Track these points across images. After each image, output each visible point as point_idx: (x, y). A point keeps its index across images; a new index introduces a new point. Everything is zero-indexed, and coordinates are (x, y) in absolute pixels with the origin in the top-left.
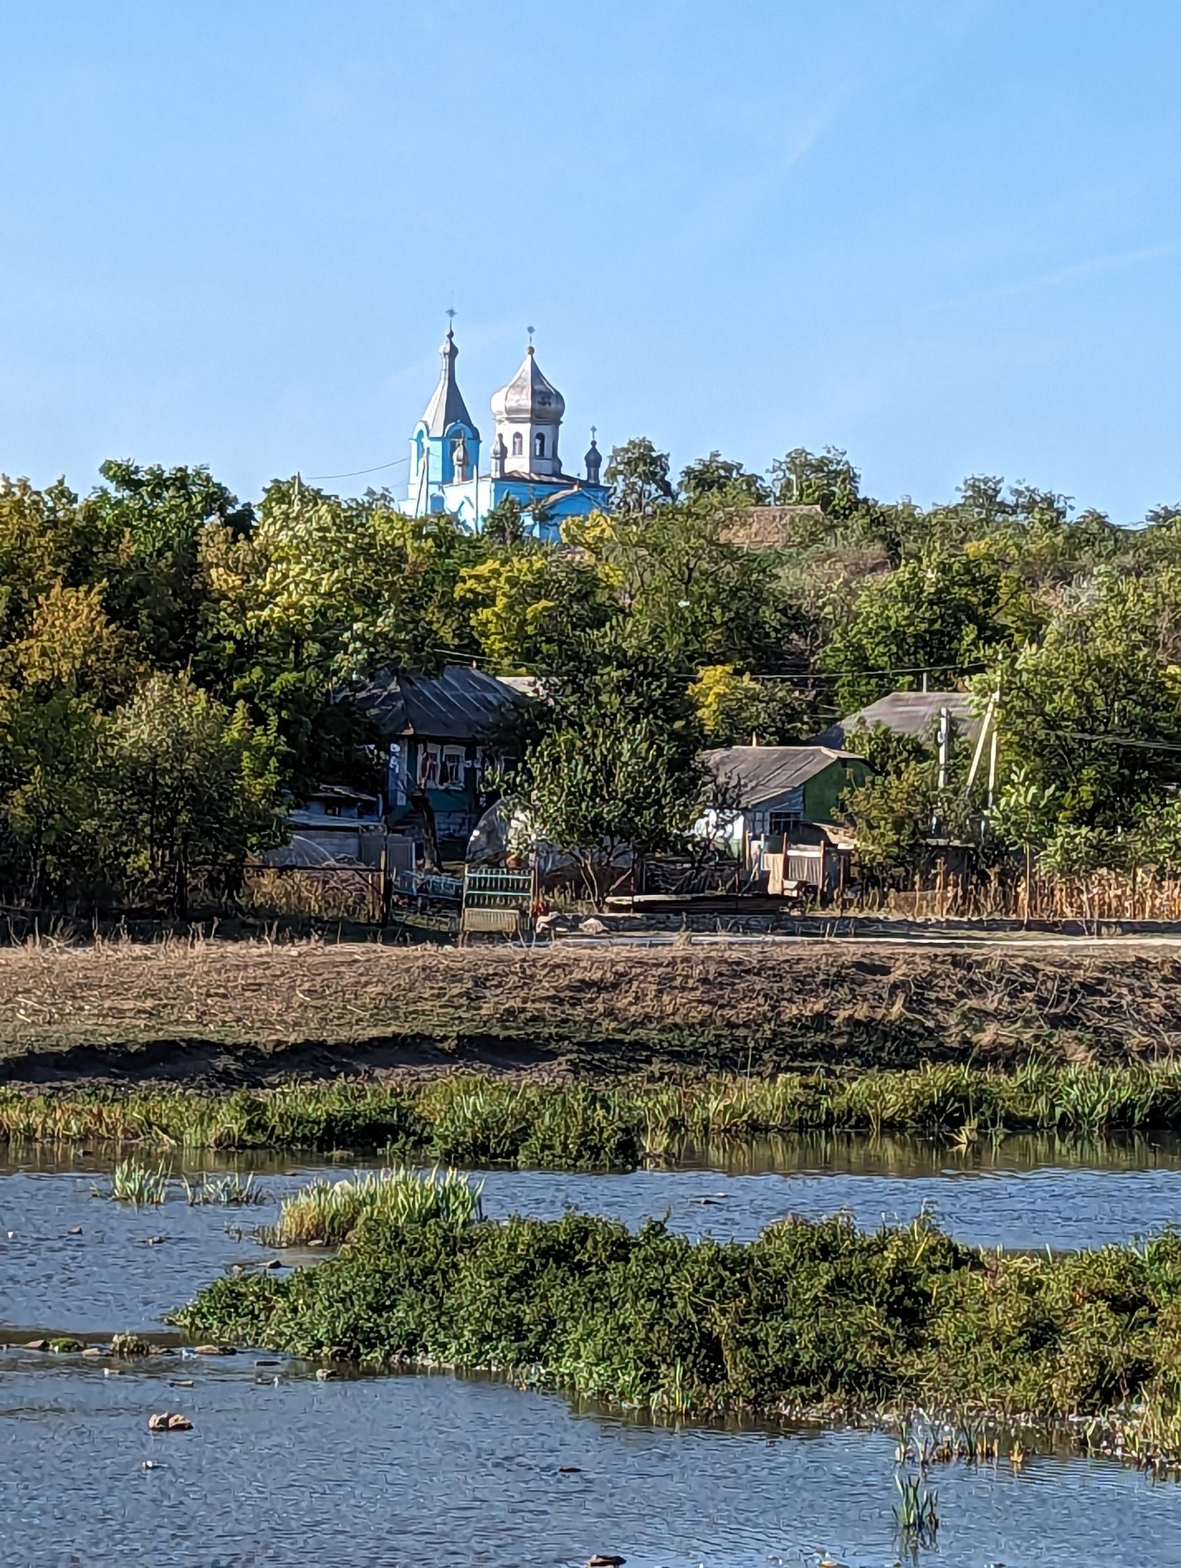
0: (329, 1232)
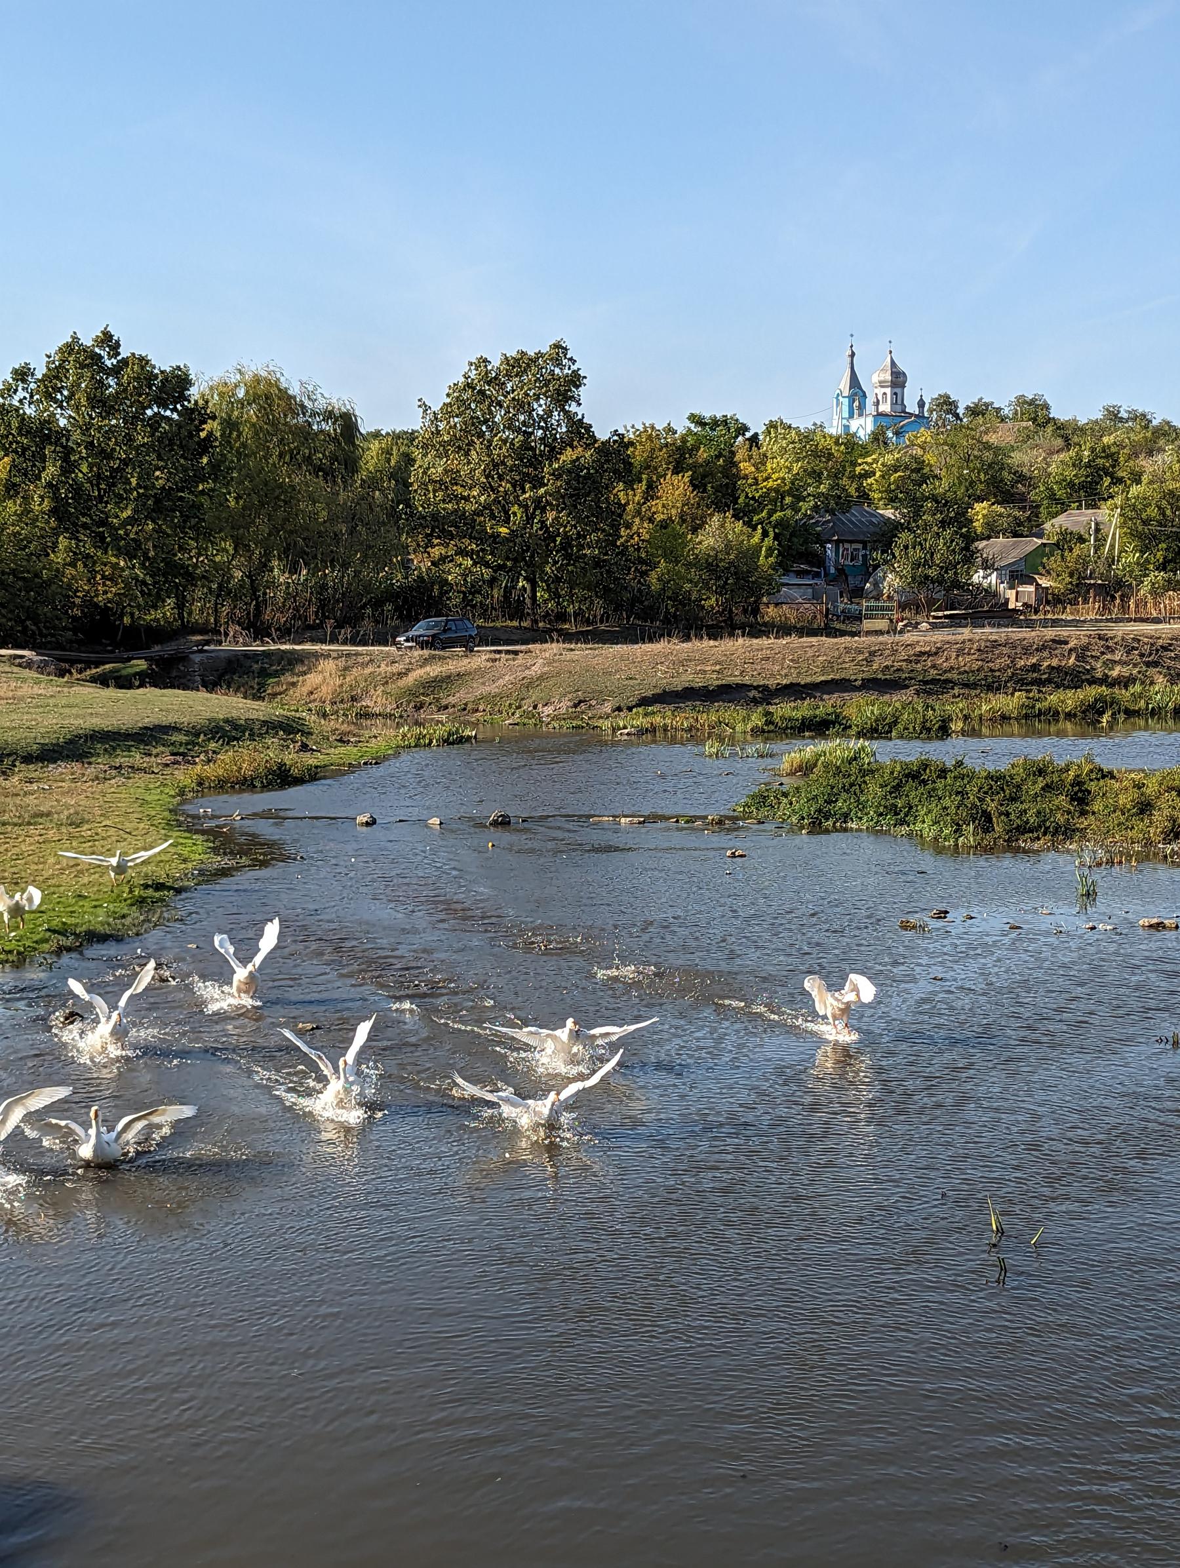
0: (805, 769)
